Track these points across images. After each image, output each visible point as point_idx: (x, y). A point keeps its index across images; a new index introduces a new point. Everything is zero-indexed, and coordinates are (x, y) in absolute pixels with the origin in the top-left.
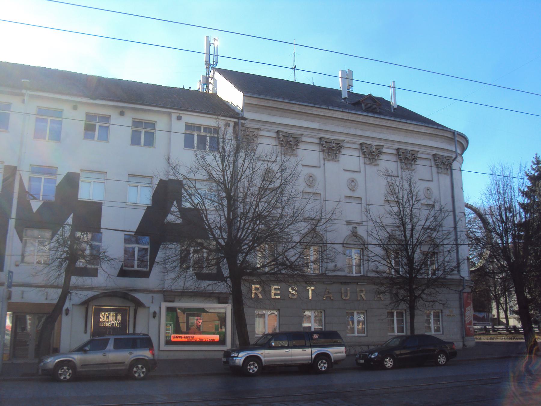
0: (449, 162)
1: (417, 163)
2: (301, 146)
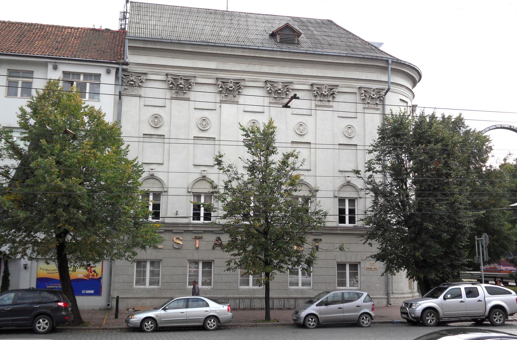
0: (380, 95)
1: (336, 100)
2: (195, 88)
